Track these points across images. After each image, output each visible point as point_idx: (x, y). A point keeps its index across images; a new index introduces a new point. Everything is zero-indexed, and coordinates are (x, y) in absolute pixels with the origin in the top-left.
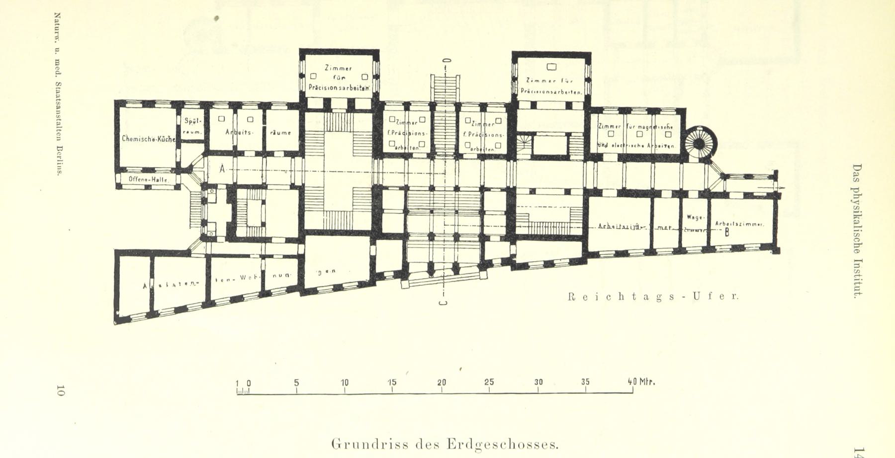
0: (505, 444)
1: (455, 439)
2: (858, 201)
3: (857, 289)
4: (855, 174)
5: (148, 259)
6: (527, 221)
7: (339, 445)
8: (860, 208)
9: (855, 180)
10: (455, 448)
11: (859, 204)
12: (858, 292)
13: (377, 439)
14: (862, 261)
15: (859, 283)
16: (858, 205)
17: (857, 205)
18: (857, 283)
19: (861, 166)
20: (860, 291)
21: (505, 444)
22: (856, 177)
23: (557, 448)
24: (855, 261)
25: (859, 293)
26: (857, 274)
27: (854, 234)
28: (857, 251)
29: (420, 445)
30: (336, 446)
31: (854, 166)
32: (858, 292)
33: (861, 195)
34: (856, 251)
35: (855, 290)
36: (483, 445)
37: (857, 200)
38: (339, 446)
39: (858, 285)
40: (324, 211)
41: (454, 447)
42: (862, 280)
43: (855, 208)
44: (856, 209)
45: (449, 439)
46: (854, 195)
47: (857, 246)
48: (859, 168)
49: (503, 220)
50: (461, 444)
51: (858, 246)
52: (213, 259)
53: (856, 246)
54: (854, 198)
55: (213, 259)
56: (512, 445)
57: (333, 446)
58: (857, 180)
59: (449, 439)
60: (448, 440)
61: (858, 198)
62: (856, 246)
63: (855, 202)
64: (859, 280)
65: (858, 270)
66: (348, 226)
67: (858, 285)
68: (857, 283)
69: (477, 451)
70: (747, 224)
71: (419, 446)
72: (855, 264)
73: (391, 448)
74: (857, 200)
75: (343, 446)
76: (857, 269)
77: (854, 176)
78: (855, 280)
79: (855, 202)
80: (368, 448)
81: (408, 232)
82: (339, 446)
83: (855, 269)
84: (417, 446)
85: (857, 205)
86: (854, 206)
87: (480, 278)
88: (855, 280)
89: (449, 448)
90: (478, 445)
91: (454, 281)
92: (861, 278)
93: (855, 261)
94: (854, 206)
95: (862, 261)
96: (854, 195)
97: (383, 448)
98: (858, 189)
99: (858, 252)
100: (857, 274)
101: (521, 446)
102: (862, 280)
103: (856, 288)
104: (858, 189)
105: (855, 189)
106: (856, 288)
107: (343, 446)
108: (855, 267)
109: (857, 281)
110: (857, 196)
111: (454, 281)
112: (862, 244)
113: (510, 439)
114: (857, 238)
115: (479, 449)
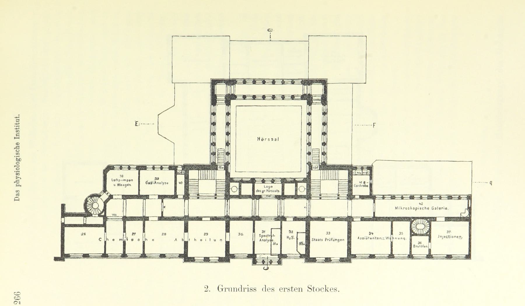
2: (16, 178)
4: (18, 195)
5: (141, 194)
6: (200, 179)
7: (222, 289)
9: (18, 191)
11: (16, 177)
12: (17, 119)
14: (15, 138)
15: (16, 124)
18: (17, 124)
19: (15, 200)
22: (17, 193)
25: (16, 118)
27: (19, 192)
28: (17, 144)
29: (265, 289)
30: (220, 290)
32: (17, 119)
33: (14, 182)
34: (18, 144)
35: (19, 120)
38: (222, 290)
39: (17, 123)
40: (320, 180)
44: (18, 131)
48: (16, 199)
50: (226, 289)
51: (17, 181)
52: (468, 223)
53: (18, 147)
55: (468, 223)
58: (17, 191)
62: (18, 147)
63: (19, 177)
64: (17, 126)
66: (191, 191)
67: (17, 123)
68: (17, 124)
70: (124, 180)
74: (17, 179)
75: (224, 290)
76: (18, 133)
77: (19, 194)
78: (19, 126)
79: (19, 177)
81: (230, 200)
82: (222, 290)
83: (18, 133)
88: (19, 126)
91: (253, 235)
92: (15, 127)
94: (19, 175)
96: (19, 182)
97: (284, 291)
98: (17, 186)
99: (17, 143)
101: (318, 290)
102: (15, 126)
103: (18, 121)
105: (19, 186)
106: (18, 121)
107: (224, 290)
109: (18, 119)
111: (253, 235)
112: (15, 148)
113: (326, 286)
114: (17, 152)
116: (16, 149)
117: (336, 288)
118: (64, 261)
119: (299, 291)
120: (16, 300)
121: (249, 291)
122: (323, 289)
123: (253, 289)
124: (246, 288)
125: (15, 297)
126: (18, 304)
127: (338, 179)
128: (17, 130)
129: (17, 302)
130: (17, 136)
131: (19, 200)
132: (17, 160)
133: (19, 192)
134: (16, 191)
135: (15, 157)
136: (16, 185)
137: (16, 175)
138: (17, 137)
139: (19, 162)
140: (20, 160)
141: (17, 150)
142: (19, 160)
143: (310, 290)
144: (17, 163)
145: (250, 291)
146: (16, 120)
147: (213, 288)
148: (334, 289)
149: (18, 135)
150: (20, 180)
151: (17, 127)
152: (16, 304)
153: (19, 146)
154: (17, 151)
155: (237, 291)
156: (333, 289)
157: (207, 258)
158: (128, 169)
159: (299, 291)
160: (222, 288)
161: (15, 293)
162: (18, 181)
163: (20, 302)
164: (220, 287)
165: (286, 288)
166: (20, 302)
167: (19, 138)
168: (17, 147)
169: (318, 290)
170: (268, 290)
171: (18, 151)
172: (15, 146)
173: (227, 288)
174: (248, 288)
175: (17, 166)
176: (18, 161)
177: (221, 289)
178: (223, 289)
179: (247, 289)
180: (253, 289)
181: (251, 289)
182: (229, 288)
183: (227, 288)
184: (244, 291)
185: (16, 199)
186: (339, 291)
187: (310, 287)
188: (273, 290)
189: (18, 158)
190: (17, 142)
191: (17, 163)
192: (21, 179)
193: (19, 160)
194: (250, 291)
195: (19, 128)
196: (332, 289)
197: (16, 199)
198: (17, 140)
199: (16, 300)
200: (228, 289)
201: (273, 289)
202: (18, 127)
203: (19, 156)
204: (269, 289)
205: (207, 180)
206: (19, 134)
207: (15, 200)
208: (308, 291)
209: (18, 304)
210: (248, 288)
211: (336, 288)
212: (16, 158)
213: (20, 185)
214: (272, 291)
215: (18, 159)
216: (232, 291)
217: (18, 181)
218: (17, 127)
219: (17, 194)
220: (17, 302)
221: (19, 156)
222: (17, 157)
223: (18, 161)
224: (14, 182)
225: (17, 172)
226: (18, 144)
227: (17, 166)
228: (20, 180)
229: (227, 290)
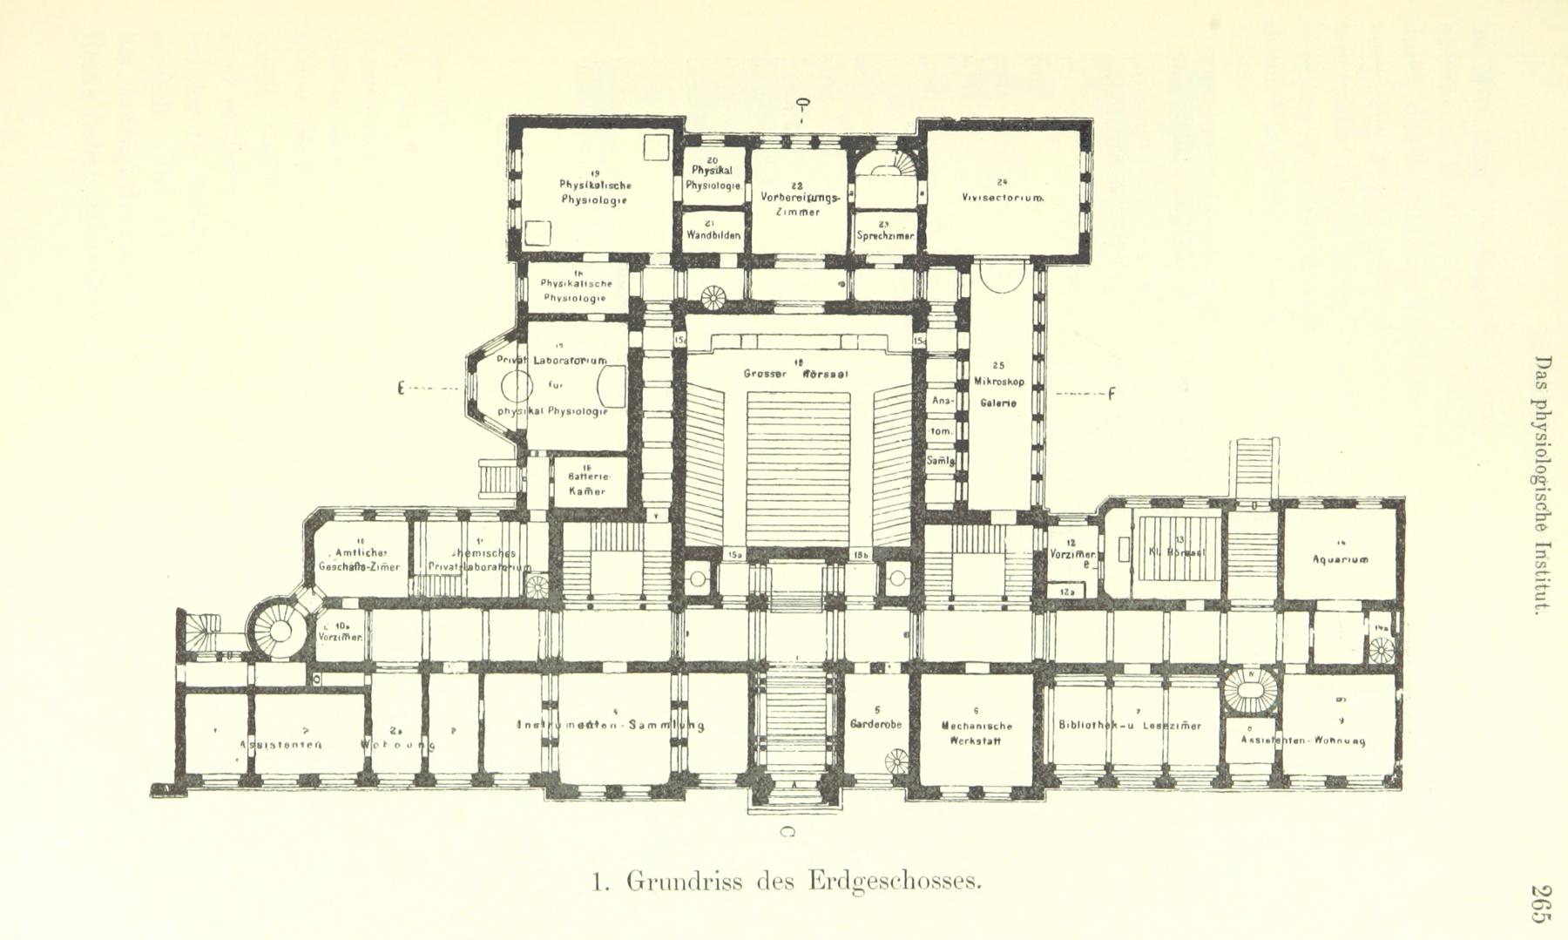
1: (823, 871)
2: (1545, 425)
3: (1540, 597)
4: (1539, 375)
7: (641, 883)
8: (1548, 438)
9: (1539, 385)
13: (767, 872)
14: (1550, 545)
15: (1545, 586)
16: (1544, 432)
17: (1541, 432)
18: (1542, 586)
19: (1550, 360)
22: (1541, 381)
24: (1537, 545)
25: (1545, 605)
26: (1541, 568)
27: (1537, 383)
28: (1542, 528)
30: (635, 885)
33: (1550, 413)
34: (1539, 528)
35: (1537, 599)
36: (865, 882)
37: (1542, 422)
38: (641, 886)
39: (1542, 590)
40: (644, 551)
41: (822, 886)
42: (1549, 580)
43: (1539, 437)
44: (1540, 439)
46: (1538, 413)
47: (1542, 517)
48: (1548, 363)
49: (647, 404)
50: (653, 882)
51: (1543, 416)
53: (1539, 517)
54: (1538, 419)
56: (909, 882)
58: (1544, 386)
60: (811, 872)
61: (1543, 520)
62: (1539, 517)
63: (1539, 427)
64: (1544, 580)
65: (1542, 563)
67: (1542, 590)
68: (1542, 586)
69: (857, 893)
71: (763, 884)
72: (1537, 552)
73: (597, 888)
74: (1542, 422)
75: (646, 885)
76: (1541, 560)
79: (1539, 427)
80: (676, 889)
82: (641, 886)
83: (1538, 559)
85: (1541, 432)
86: (1537, 434)
87: (481, 492)
89: (813, 887)
90: (858, 881)
92: (1547, 576)
93: (1537, 545)
94: (1537, 434)
95: (1550, 545)
96: (1538, 413)
97: (651, 889)
98: (1544, 402)
99: (1542, 530)
100: (1541, 568)
101: (924, 883)
102: (1549, 580)
103: (1539, 596)
105: (1538, 402)
106: (1539, 596)
107: (646, 885)
108: (1537, 557)
109: (1540, 583)
114: (1541, 504)
115: (861, 890)
116: (1544, 512)
117: (741, 880)
118: (510, 259)
119: (906, 887)
120: (1545, 898)
121: (720, 887)
122: (899, 880)
124: (712, 880)
125: (1548, 908)
126: (1539, 887)
127: (589, 554)
128: (1541, 569)
129: (1541, 893)
130: (1544, 552)
132: (1542, 480)
134: (1545, 387)
135: (1549, 489)
136: (1547, 403)
139: (1536, 474)
142: (1539, 478)
144: (1542, 469)
148: (784, 881)
150: (1534, 420)
151: (1542, 576)
152: (1545, 888)
153: (1537, 520)
154: (1544, 506)
155: (913, 887)
156: (876, 881)
157: (976, 787)
158: (1036, 323)
159: (906, 887)
161: (1548, 905)
163: (1534, 893)
165: (835, 880)
166: (1534, 893)
168: (1543, 517)
169: (924, 883)
170: (690, 885)
171: (1543, 453)
172: (1548, 521)
173: (656, 881)
174: (718, 880)
175: (1542, 460)
178: (644, 884)
179: (715, 881)
180: (942, 882)
181: (727, 881)
182: (662, 880)
183: (656, 881)
184: (706, 888)
185: (1546, 363)
188: (729, 885)
189: (1539, 485)
191: (1542, 469)
192: (1532, 423)
193: (1539, 478)
195: (1537, 606)
196: (959, 880)
197: (1546, 363)
199: (1545, 898)
200: (659, 881)
201: (970, 882)
203: (1537, 490)
204: (778, 880)
205: (988, 555)
207: (1550, 360)
209: (1539, 887)
210: (718, 880)
211: (741, 880)
213: (1534, 404)
214: (881, 887)
215: (1542, 482)
216: (698, 888)
218: (1542, 576)
219: (1542, 377)
220: (1541, 893)
221: (1537, 490)
222: (1544, 489)
225: (1545, 444)
227: (1542, 460)
228: (1534, 420)
229: (656, 886)
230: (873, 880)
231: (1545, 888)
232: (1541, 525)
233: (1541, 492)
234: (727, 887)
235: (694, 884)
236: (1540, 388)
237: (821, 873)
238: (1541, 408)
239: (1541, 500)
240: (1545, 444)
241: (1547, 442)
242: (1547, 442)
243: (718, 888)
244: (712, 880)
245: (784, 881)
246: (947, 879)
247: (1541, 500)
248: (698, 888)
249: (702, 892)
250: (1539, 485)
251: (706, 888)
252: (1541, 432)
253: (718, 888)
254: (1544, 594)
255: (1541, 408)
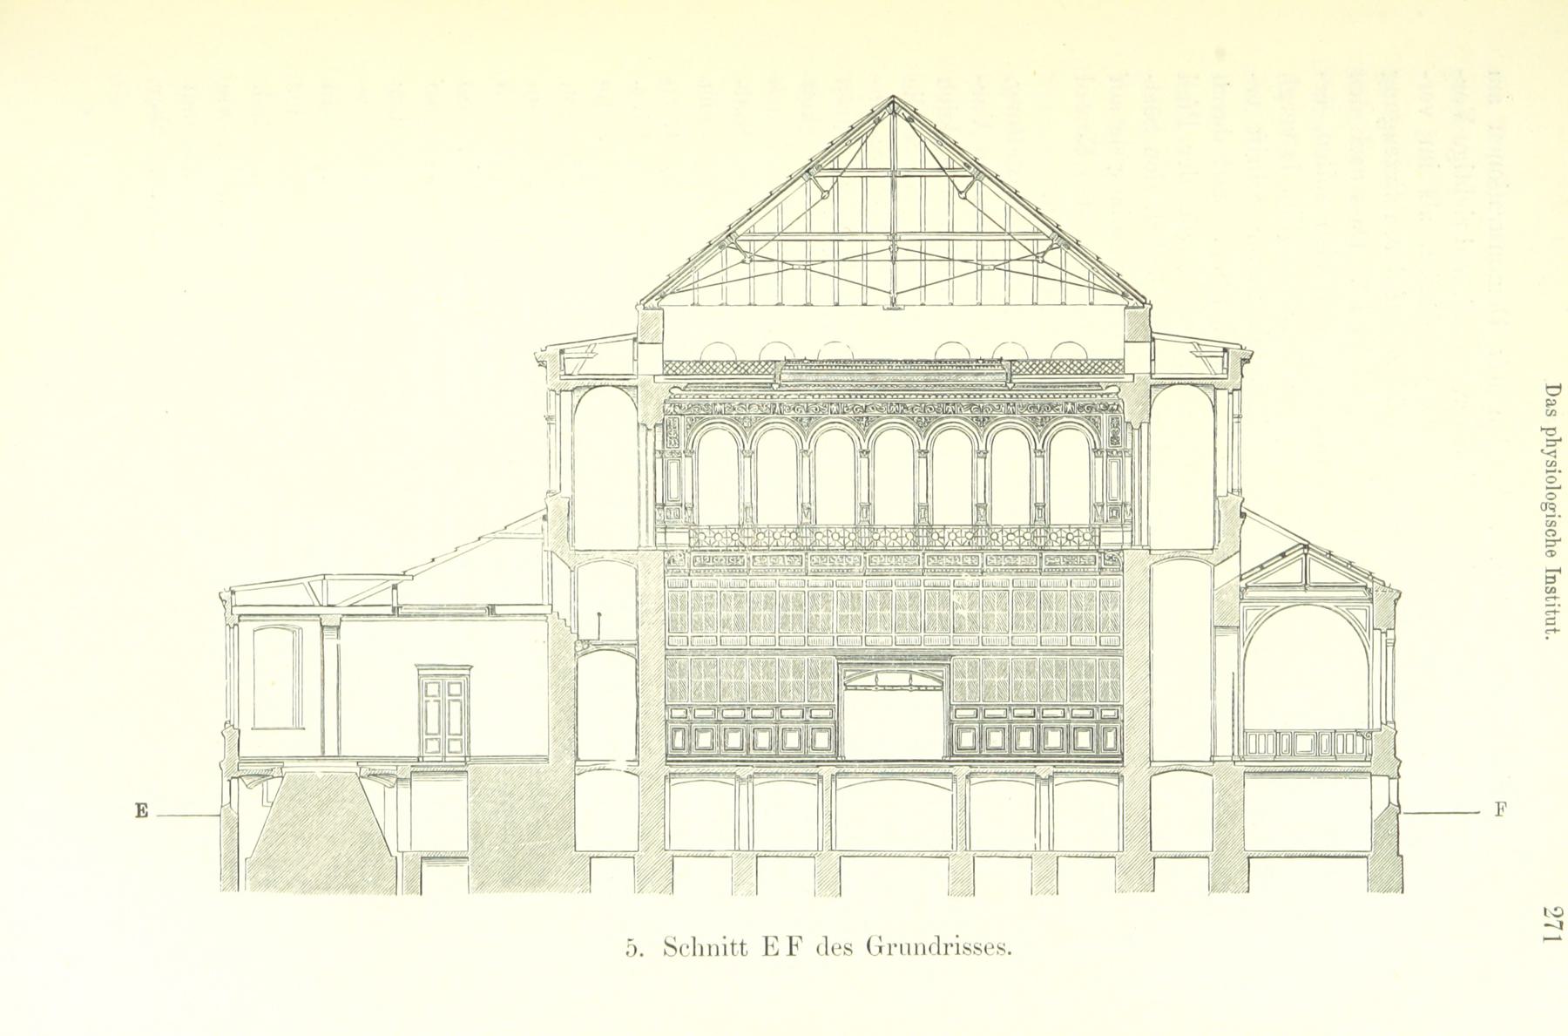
0: (627, 953)
1: (801, 937)
2: (1555, 452)
4: (1549, 402)
7: (880, 948)
9: (1549, 413)
10: (777, 954)
11: (1555, 457)
12: (1552, 627)
13: (826, 938)
14: (1560, 571)
15: (1555, 612)
16: (1554, 459)
17: (1552, 459)
19: (1560, 387)
20: (1557, 627)
21: (627, 953)
22: (1552, 408)
23: (1010, 953)
25: (1555, 630)
28: (1552, 554)
30: (875, 950)
31: (1548, 387)
32: (1552, 627)
34: (1549, 554)
35: (1547, 624)
37: (1552, 449)
38: (880, 951)
39: (1552, 615)
41: (775, 952)
42: (1559, 605)
43: (1549, 464)
44: (1548, 593)
45: (791, 938)
46: (1547, 440)
48: (1557, 391)
50: (893, 946)
51: (1553, 443)
53: (1549, 543)
54: (1548, 446)
57: (869, 950)
58: (1552, 414)
59: (791, 938)
60: (764, 939)
61: (1554, 446)
62: (1549, 543)
63: (1548, 454)
64: (1554, 605)
65: (1552, 522)
67: (1552, 615)
71: (822, 950)
73: (1545, 939)
74: (1552, 449)
75: (885, 950)
76: (1551, 586)
77: (1548, 405)
78: (1547, 605)
79: (1548, 454)
82: (880, 951)
83: (1548, 585)
84: (818, 950)
88: (1547, 605)
89: (767, 954)
92: (1557, 602)
95: (1560, 571)
96: (1547, 440)
97: (890, 954)
98: (1554, 429)
99: (1552, 556)
102: (1559, 605)
104: (1554, 429)
107: (885, 950)
109: (1552, 608)
110: (1553, 443)
119: (694, 954)
121: (961, 952)
122: (688, 947)
123: (972, 945)
124: (952, 945)
126: (1551, 909)
128: (1552, 595)
130: (1554, 578)
131: (1548, 387)
132: (1552, 506)
133: (1547, 410)
135: (1560, 471)
137: (1556, 460)
138: (1551, 577)
139: (1546, 501)
140: (1544, 507)
141: (1553, 535)
142: (1549, 506)
143: (670, 951)
144: (1552, 496)
145: (964, 953)
146: (1554, 624)
147: (652, 946)
148: (843, 947)
149: (1549, 580)
150: (1544, 447)
151: (1552, 601)
153: (1547, 546)
159: (694, 954)
160: (880, 945)
162: (1550, 443)
164: (875, 943)
167: (1547, 571)
172: (1557, 548)
173: (896, 946)
175: (1552, 488)
176: (1550, 502)
177: (878, 949)
178: (883, 949)
179: (955, 946)
180: (973, 949)
181: (967, 946)
182: (901, 945)
183: (896, 946)
184: (946, 953)
185: (1556, 391)
186: (642, 955)
187: (671, 941)
189: (1550, 512)
190: (1551, 558)
191: (1552, 496)
192: (1542, 450)
193: (1549, 506)
194: (964, 953)
196: (989, 946)
198: (1553, 563)
202: (1548, 603)
203: (1547, 516)
204: (836, 946)
206: (1547, 583)
208: (665, 953)
209: (1551, 909)
212: (1557, 513)
213: (1544, 431)
214: (998, 953)
216: (938, 953)
217: (1550, 443)
218: (1552, 601)
219: (1552, 405)
221: (1547, 516)
223: (1550, 502)
224: (1560, 440)
225: (1554, 471)
226: (1549, 554)
227: (1552, 488)
229: (896, 951)
230: (838, 946)
231: (1556, 909)
232: (1551, 551)
233: (1551, 519)
234: (966, 951)
235: (935, 949)
236: (1550, 415)
237: (775, 939)
238: (1550, 435)
239: (1551, 526)
240: (1554, 471)
241: (1558, 468)
242: (1558, 468)
243: (958, 953)
244: (952, 945)
245: (843, 947)
246: (978, 946)
247: (1551, 526)
248: (938, 953)
249: (942, 956)
250: (1550, 512)
251: (946, 953)
252: (1551, 459)
253: (958, 953)
254: (1554, 619)
255: (1550, 435)
